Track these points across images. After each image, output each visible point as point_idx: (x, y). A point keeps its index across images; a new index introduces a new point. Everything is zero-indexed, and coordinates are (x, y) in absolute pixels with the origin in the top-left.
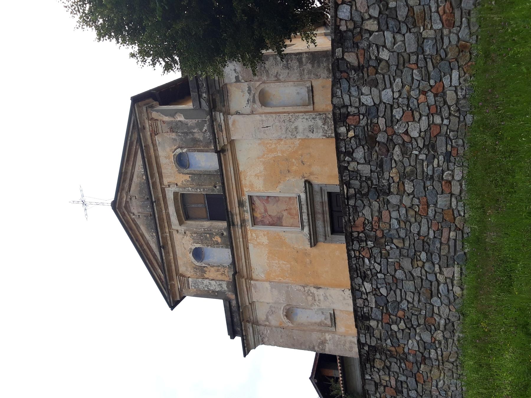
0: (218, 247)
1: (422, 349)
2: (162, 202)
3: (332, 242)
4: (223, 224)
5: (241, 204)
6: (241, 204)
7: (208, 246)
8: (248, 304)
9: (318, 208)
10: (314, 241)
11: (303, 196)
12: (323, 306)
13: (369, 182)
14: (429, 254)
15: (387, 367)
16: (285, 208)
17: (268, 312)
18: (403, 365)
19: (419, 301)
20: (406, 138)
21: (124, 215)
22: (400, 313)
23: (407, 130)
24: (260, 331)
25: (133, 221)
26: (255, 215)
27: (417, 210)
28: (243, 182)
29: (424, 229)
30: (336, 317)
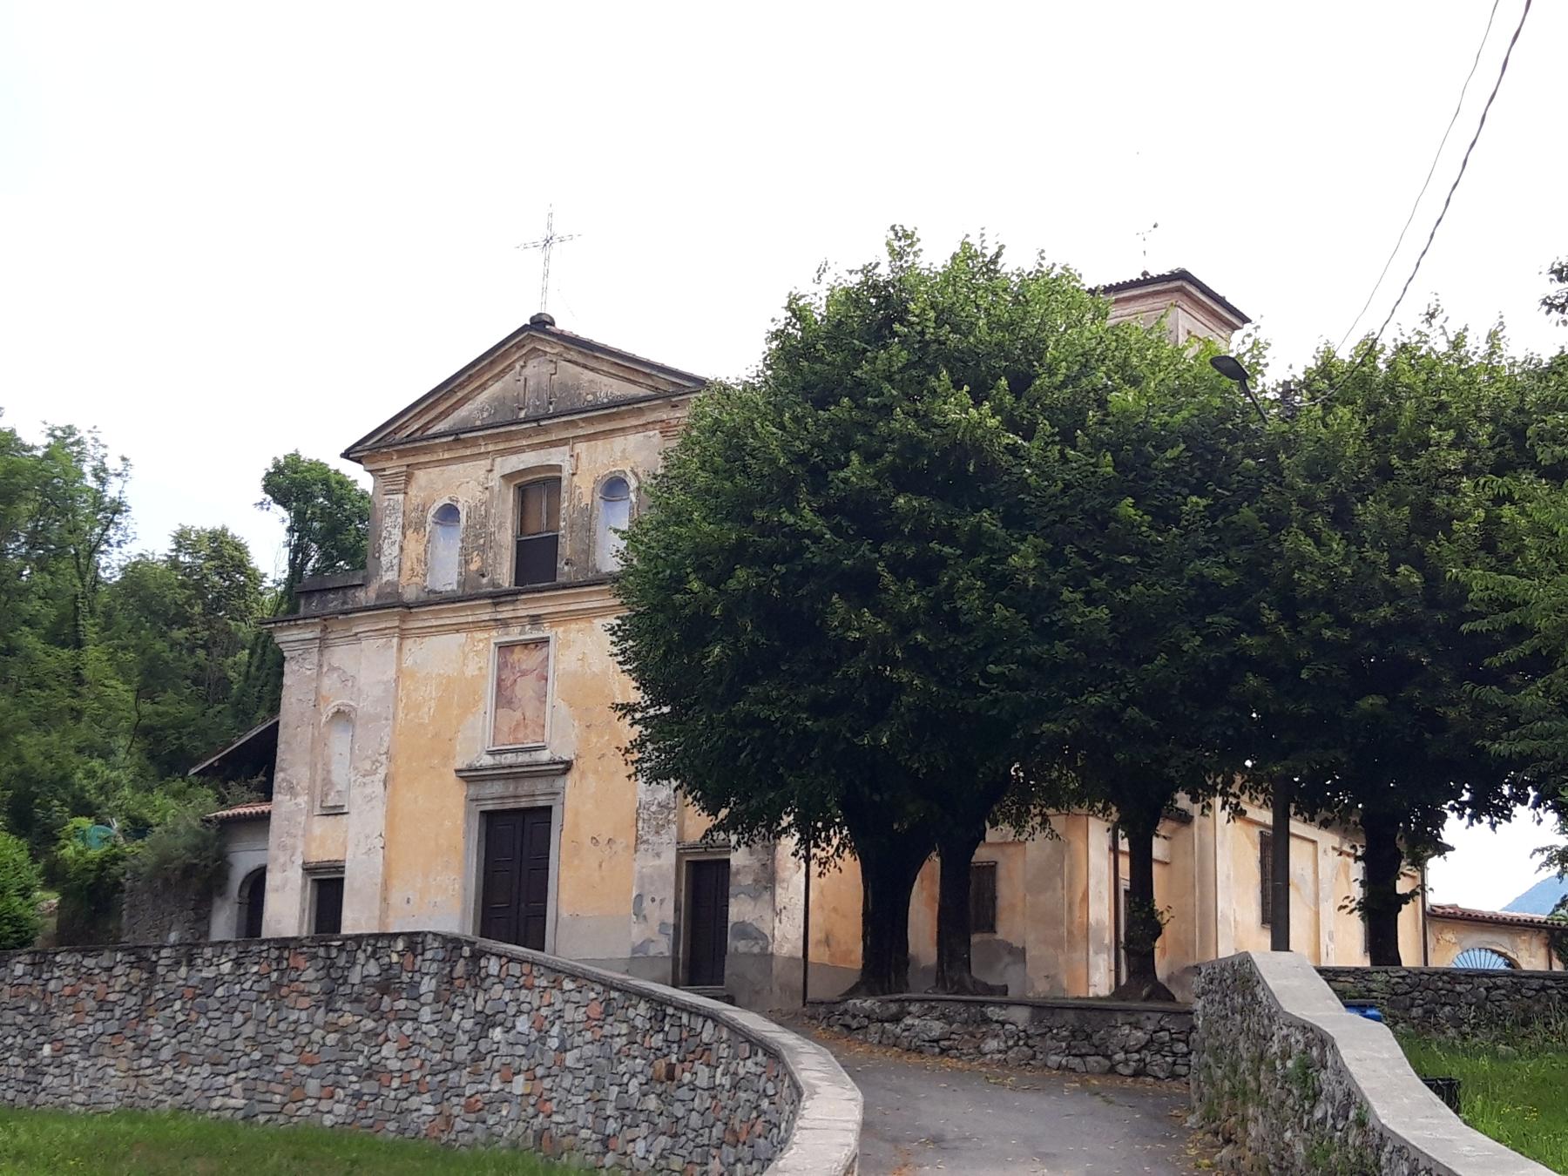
0: (460, 566)
1: (152, 1045)
2: (542, 439)
3: (468, 813)
4: (505, 575)
5: (535, 620)
6: (535, 620)
7: (463, 541)
8: (355, 630)
9: (526, 786)
10: (471, 776)
11: (544, 756)
12: (355, 792)
13: (341, 981)
14: (258, 1064)
15: (131, 989)
16: (527, 714)
17: (344, 672)
18: (133, 1015)
19: (207, 1045)
20: (382, 1038)
21: (519, 346)
22: (194, 1016)
23: (389, 1040)
24: (310, 653)
25: (509, 365)
26: (517, 649)
27: (307, 1049)
28: (574, 626)
29: (285, 1058)
30: (339, 817)
